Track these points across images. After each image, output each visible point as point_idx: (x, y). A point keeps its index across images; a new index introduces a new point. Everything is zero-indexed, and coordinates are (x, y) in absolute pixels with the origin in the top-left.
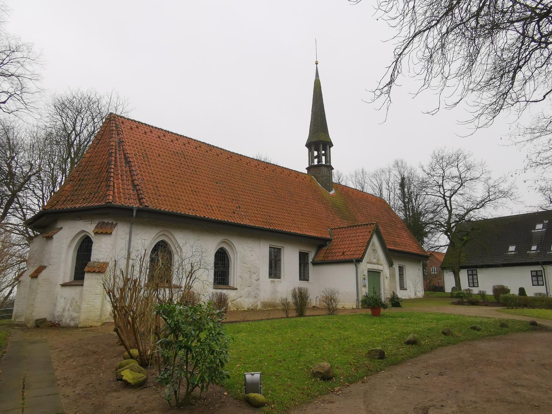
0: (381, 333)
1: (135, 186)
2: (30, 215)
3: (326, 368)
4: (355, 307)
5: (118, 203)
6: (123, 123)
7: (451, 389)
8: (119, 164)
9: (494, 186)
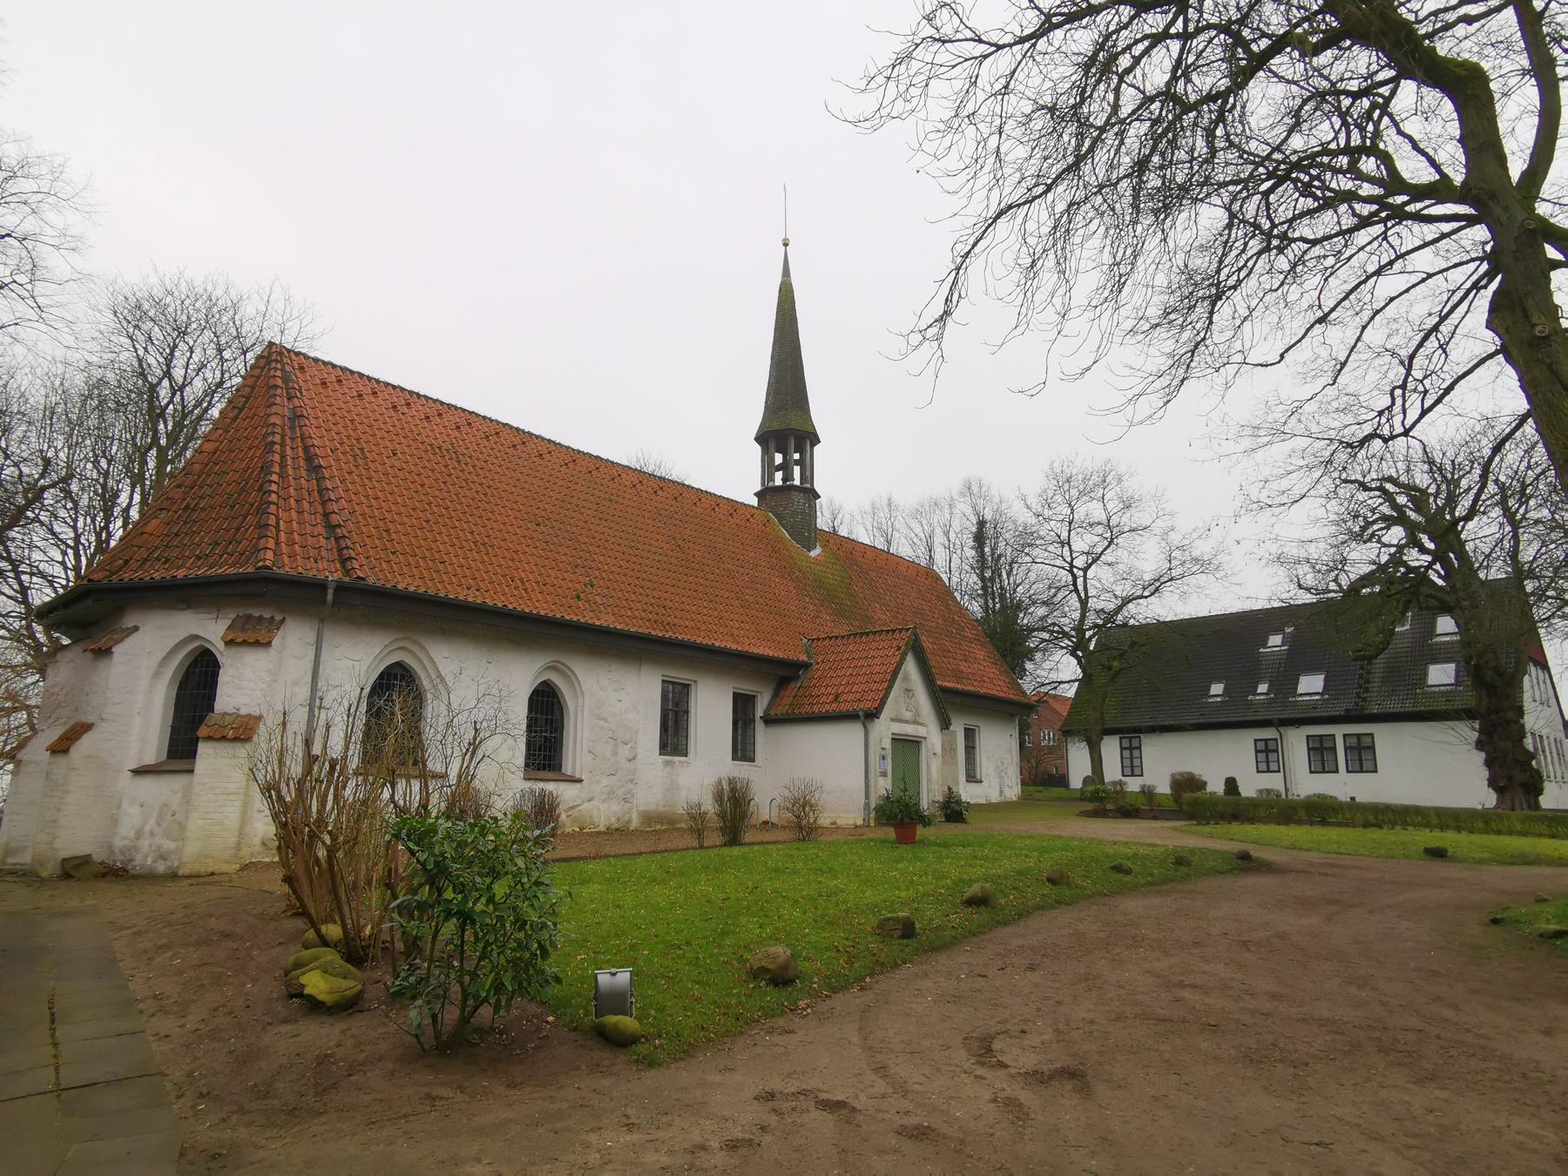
0: (911, 882)
1: (331, 527)
2: (41, 595)
3: (781, 960)
4: (860, 822)
5: (287, 569)
6: (301, 368)
7: (1048, 998)
8: (290, 472)
9: (1181, 548)
